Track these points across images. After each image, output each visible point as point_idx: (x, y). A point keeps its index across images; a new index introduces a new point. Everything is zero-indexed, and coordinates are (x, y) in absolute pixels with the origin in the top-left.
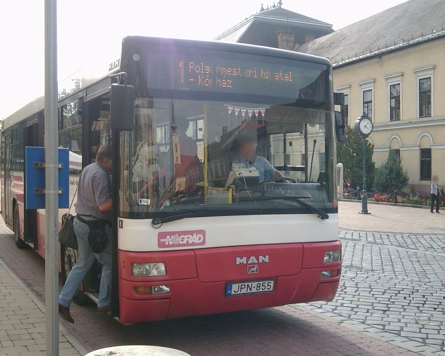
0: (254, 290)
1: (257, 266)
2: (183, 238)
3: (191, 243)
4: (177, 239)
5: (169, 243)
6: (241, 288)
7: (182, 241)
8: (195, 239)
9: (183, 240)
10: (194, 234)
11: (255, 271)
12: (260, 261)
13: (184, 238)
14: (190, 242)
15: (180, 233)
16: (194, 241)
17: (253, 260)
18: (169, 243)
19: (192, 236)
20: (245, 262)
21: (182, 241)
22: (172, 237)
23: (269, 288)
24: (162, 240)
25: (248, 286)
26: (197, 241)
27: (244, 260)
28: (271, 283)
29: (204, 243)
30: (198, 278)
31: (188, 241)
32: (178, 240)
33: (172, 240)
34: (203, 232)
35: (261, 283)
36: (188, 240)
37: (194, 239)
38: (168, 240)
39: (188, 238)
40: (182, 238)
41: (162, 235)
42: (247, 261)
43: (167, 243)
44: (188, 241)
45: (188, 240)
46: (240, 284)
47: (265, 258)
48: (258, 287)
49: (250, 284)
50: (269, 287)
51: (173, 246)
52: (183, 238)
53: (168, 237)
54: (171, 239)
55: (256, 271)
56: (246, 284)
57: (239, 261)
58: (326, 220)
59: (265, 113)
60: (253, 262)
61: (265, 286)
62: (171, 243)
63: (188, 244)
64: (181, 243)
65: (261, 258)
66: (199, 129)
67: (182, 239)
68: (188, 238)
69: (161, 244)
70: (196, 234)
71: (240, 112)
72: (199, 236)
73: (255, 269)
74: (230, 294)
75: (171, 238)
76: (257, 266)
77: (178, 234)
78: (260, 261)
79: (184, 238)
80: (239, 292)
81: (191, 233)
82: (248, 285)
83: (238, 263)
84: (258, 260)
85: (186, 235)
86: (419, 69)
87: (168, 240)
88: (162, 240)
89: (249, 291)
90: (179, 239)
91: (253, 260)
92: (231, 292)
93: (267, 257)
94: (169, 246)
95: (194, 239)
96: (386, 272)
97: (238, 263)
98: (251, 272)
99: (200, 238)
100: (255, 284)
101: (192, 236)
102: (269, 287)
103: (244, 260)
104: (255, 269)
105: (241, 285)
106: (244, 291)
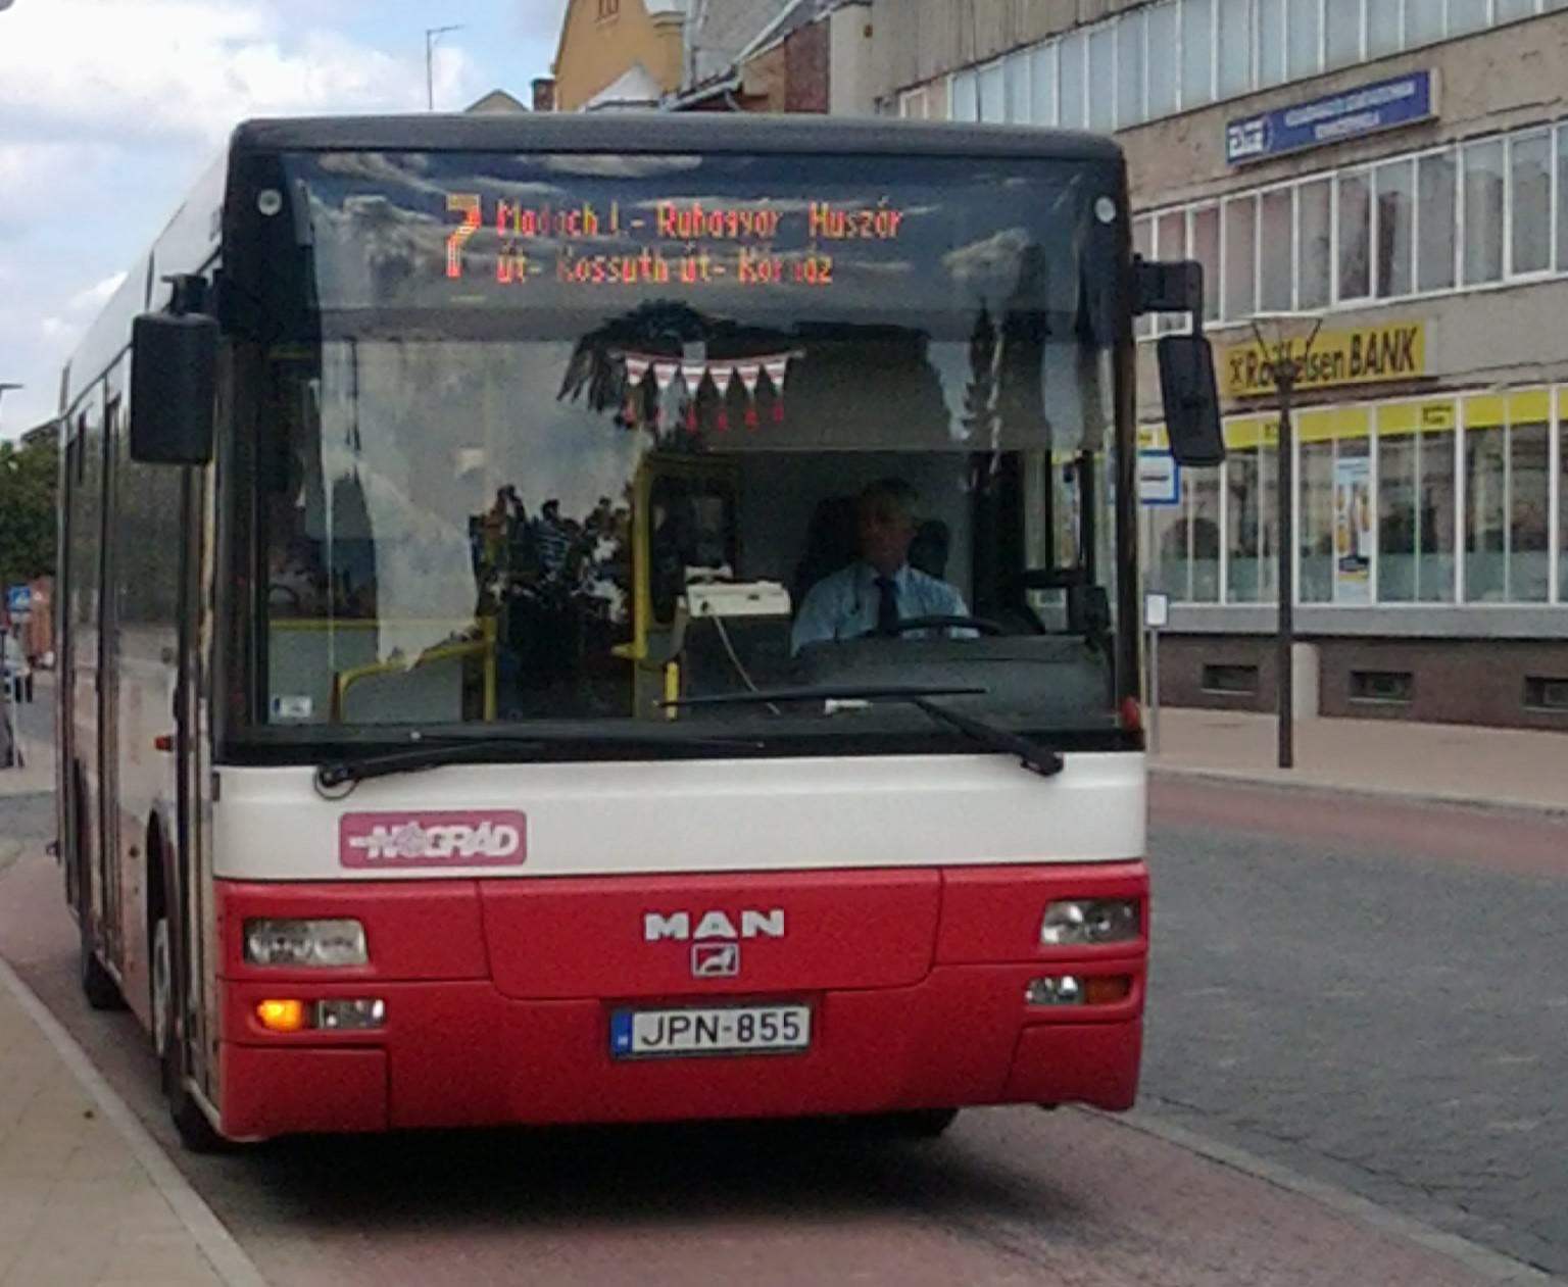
0: (728, 1040)
2: (438, 838)
6: (673, 1031)
7: (436, 845)
8: (489, 840)
14: (466, 852)
15: (426, 819)
16: (478, 849)
24: (355, 842)
25: (700, 1022)
26: (493, 850)
27: (679, 925)
29: (519, 857)
31: (456, 850)
32: (420, 842)
34: (517, 819)
35: (757, 1013)
38: (377, 841)
39: (459, 837)
41: (353, 825)
42: (693, 925)
43: (373, 854)
44: (456, 850)
46: (667, 1015)
49: (708, 1016)
51: (400, 862)
53: (379, 831)
54: (392, 839)
56: (692, 1016)
57: (655, 927)
63: (455, 859)
64: (430, 852)
65: (751, 922)
68: (459, 837)
69: (348, 857)
72: (501, 830)
73: (725, 959)
80: (664, 1045)
81: (472, 819)
83: (651, 934)
84: (737, 925)
87: (377, 841)
93: (778, 916)
94: (382, 862)
97: (651, 934)
99: (505, 840)
100: (729, 1017)
103: (679, 925)
104: (725, 959)
106: (685, 1041)
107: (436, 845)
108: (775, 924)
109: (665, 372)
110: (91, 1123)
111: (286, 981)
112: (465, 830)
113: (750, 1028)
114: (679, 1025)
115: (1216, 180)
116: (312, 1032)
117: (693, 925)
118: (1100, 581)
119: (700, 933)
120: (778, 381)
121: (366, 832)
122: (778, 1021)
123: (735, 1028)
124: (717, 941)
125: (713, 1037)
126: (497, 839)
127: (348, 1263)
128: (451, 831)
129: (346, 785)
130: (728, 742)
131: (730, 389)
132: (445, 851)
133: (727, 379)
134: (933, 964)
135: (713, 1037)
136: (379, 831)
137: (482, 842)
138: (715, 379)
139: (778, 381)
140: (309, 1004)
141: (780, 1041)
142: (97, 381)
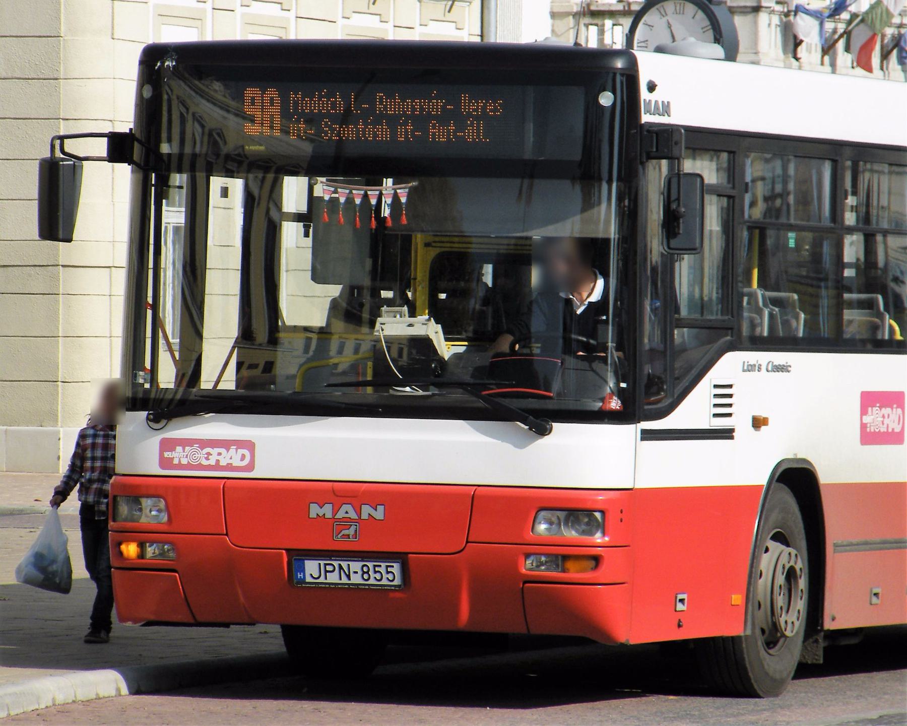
0: (356, 579)
1: (356, 525)
2: (209, 454)
3: (225, 464)
4: (197, 455)
5: (180, 461)
6: (326, 572)
7: (207, 459)
8: (233, 457)
9: (208, 457)
10: (232, 447)
11: (351, 536)
12: (365, 516)
13: (211, 455)
14: (223, 463)
15: (204, 443)
16: (230, 461)
17: (347, 513)
18: (180, 461)
19: (228, 452)
20: (329, 515)
21: (207, 459)
22: (187, 448)
23: (391, 579)
24: (166, 454)
25: (341, 567)
26: (237, 462)
27: (327, 510)
28: (393, 566)
29: (250, 467)
30: (227, 534)
31: (218, 461)
32: (199, 456)
33: (187, 455)
34: (249, 445)
35: (370, 565)
36: (219, 458)
37: (231, 458)
38: (178, 455)
39: (219, 454)
40: (206, 454)
41: (167, 445)
42: (335, 512)
43: (176, 462)
44: (218, 461)
45: (219, 458)
46: (322, 563)
47: (376, 510)
48: (364, 573)
49: (344, 564)
50: (390, 577)
51: (189, 467)
52: (209, 454)
53: (179, 449)
54: (185, 454)
55: (355, 536)
56: (336, 564)
57: (315, 510)
58: (546, 439)
59: (409, 196)
60: (347, 515)
61: (379, 572)
62: (184, 461)
63: (217, 467)
64: (205, 462)
65: (366, 510)
66: (308, 237)
67: (206, 456)
68: (219, 454)
69: (165, 463)
70: (235, 447)
71: (366, 197)
72: (241, 451)
73: (351, 532)
74: (303, 581)
75: (184, 452)
76: (356, 525)
77: (197, 445)
78: (365, 516)
79: (211, 455)
80: (322, 580)
81: (226, 444)
82: (340, 565)
83: (313, 515)
84: (359, 513)
85: (215, 449)
86: (770, 39)
87: (178, 455)
88: (166, 454)
89: (344, 580)
90: (199, 456)
91: (347, 513)
92: (304, 576)
93: (381, 508)
94: (180, 466)
95: (231, 458)
96: (3, 471)
97: (313, 515)
98: (341, 537)
99: (243, 457)
100: (356, 566)
101: (228, 452)
102: (390, 577)
103: (327, 510)
104: (351, 532)
105: (326, 565)
106: (333, 578)
108: (379, 514)
109: (373, 194)
110: (837, 617)
111: (871, 544)
113: (368, 573)
114: (329, 568)
116: (143, 561)
117: (335, 512)
119: (340, 515)
120: (403, 200)
121: (172, 449)
122: (382, 570)
123: (360, 573)
124: (347, 522)
125: (349, 577)
129: (163, 422)
130: (207, 399)
131: (361, 202)
132: (212, 462)
133: (361, 196)
134: (467, 542)
135: (349, 577)
138: (370, 197)
139: (403, 200)
140: (142, 546)
141: (384, 582)
142: (268, 202)
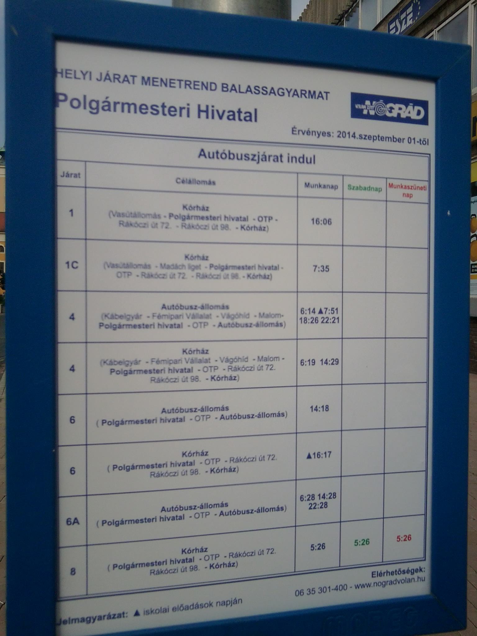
2: (392, 108)
7: (390, 112)
14: (403, 116)
31: (399, 115)
43: (365, 112)
44: (399, 115)
64: (388, 114)
68: (400, 109)
99: (419, 113)
107: (390, 112)
112: (403, 107)
115: (219, 379)
118: (412, 9)
123: (307, 320)
126: (416, 112)
127: (4, 428)
128: (396, 106)
132: (394, 114)
136: (368, 103)
137: (409, 113)
